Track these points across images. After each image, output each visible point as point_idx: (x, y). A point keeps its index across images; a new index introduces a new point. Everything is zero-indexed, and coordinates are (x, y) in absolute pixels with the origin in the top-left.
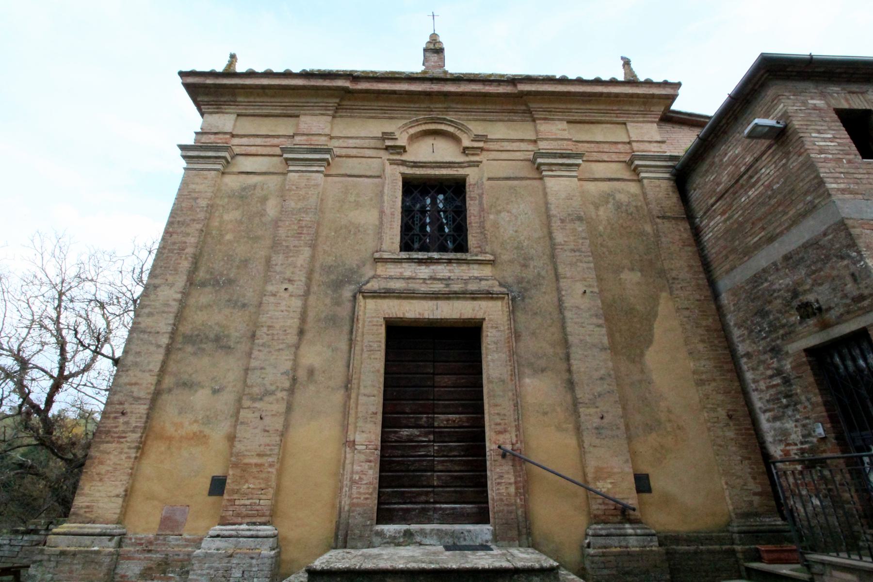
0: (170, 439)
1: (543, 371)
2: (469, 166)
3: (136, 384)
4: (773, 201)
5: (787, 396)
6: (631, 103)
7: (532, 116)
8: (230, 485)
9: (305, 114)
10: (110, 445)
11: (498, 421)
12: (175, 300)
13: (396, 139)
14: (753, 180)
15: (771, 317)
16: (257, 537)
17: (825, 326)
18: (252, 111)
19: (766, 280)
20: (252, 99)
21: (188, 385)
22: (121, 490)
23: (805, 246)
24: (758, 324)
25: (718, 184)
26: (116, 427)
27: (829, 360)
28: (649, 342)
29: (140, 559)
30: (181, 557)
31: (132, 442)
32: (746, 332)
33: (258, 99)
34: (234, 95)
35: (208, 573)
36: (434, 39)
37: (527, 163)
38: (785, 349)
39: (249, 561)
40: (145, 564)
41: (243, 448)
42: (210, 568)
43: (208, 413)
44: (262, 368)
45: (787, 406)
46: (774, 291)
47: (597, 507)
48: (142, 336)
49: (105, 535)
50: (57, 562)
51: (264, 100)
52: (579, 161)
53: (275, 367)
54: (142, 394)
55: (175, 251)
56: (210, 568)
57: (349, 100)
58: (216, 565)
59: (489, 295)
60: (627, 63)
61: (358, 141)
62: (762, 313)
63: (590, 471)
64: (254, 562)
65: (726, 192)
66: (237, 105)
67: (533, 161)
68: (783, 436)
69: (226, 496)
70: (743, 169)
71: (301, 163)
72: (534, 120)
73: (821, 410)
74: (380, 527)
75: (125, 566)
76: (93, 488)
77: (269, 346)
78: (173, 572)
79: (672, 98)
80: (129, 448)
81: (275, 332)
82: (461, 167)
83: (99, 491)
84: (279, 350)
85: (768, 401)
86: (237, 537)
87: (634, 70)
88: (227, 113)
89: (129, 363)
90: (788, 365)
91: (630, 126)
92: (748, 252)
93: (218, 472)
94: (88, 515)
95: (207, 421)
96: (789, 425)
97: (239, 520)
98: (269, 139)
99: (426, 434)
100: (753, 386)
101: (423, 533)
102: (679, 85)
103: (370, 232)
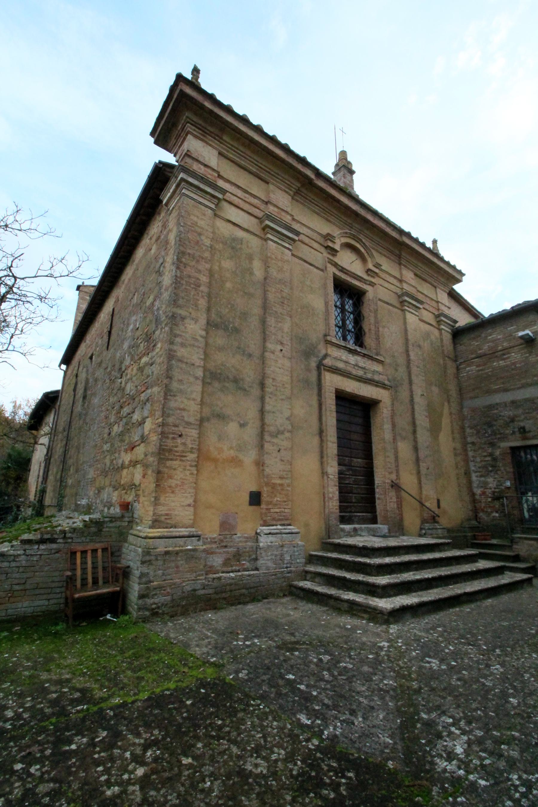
0: (215, 461)
1: (405, 439)
2: (369, 285)
3: (184, 410)
4: (513, 372)
5: (492, 466)
6: (443, 276)
7: (400, 261)
8: (265, 497)
9: (273, 184)
10: (175, 462)
11: (389, 466)
12: (201, 336)
13: (334, 243)
14: (505, 357)
15: (495, 428)
16: (292, 533)
17: (525, 438)
18: (231, 156)
19: (497, 409)
20: (235, 144)
21: (221, 417)
22: (190, 501)
23: (526, 400)
24: (485, 429)
25: (480, 349)
26: (176, 447)
27: (518, 453)
28: (441, 430)
29: (220, 553)
30: (247, 549)
31: (192, 461)
32: (475, 432)
33: (241, 148)
34: (222, 130)
35: (272, 559)
36: (343, 155)
37: (393, 294)
38: (498, 445)
39: (292, 548)
40: (225, 556)
41: (270, 472)
42: (272, 555)
43: (239, 442)
44: (273, 412)
45: (491, 471)
46: (500, 416)
47: (426, 515)
48: (180, 364)
49: (193, 537)
50: (164, 561)
51: (260, 161)
52: (421, 307)
53: (282, 413)
54: (192, 420)
55: (192, 286)
56: (272, 555)
57: (306, 189)
58: (275, 553)
59: (384, 386)
60: (435, 242)
61: (309, 231)
62: (490, 425)
63: (423, 496)
64: (296, 549)
65: (486, 355)
66: (221, 143)
67: (399, 297)
68: (485, 485)
69: (263, 506)
70: (500, 348)
71: (275, 234)
72: (400, 264)
73: (511, 475)
74: (342, 526)
75: (211, 559)
76: (167, 499)
77: (275, 395)
78: (244, 560)
79: (459, 281)
80: (191, 466)
81: (278, 385)
82: (365, 284)
83: (174, 502)
84: (282, 400)
85: (479, 467)
86: (281, 533)
87: (439, 249)
88: (210, 145)
89: (175, 390)
90: (497, 453)
91: (438, 290)
92: (489, 392)
93: (254, 488)
94: (168, 521)
95: (240, 448)
96: (490, 480)
97: (274, 523)
98: (247, 196)
99: (348, 470)
100: (472, 459)
101: (361, 529)
102: (464, 275)
103: (320, 316)
